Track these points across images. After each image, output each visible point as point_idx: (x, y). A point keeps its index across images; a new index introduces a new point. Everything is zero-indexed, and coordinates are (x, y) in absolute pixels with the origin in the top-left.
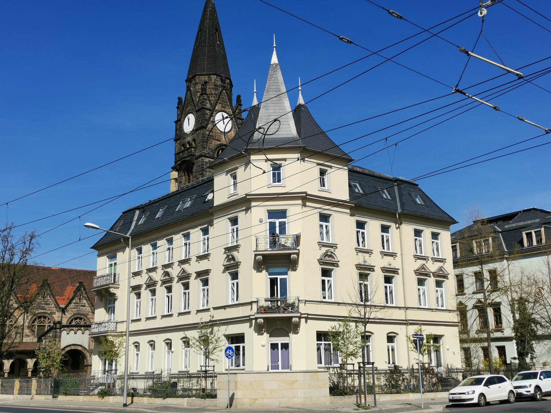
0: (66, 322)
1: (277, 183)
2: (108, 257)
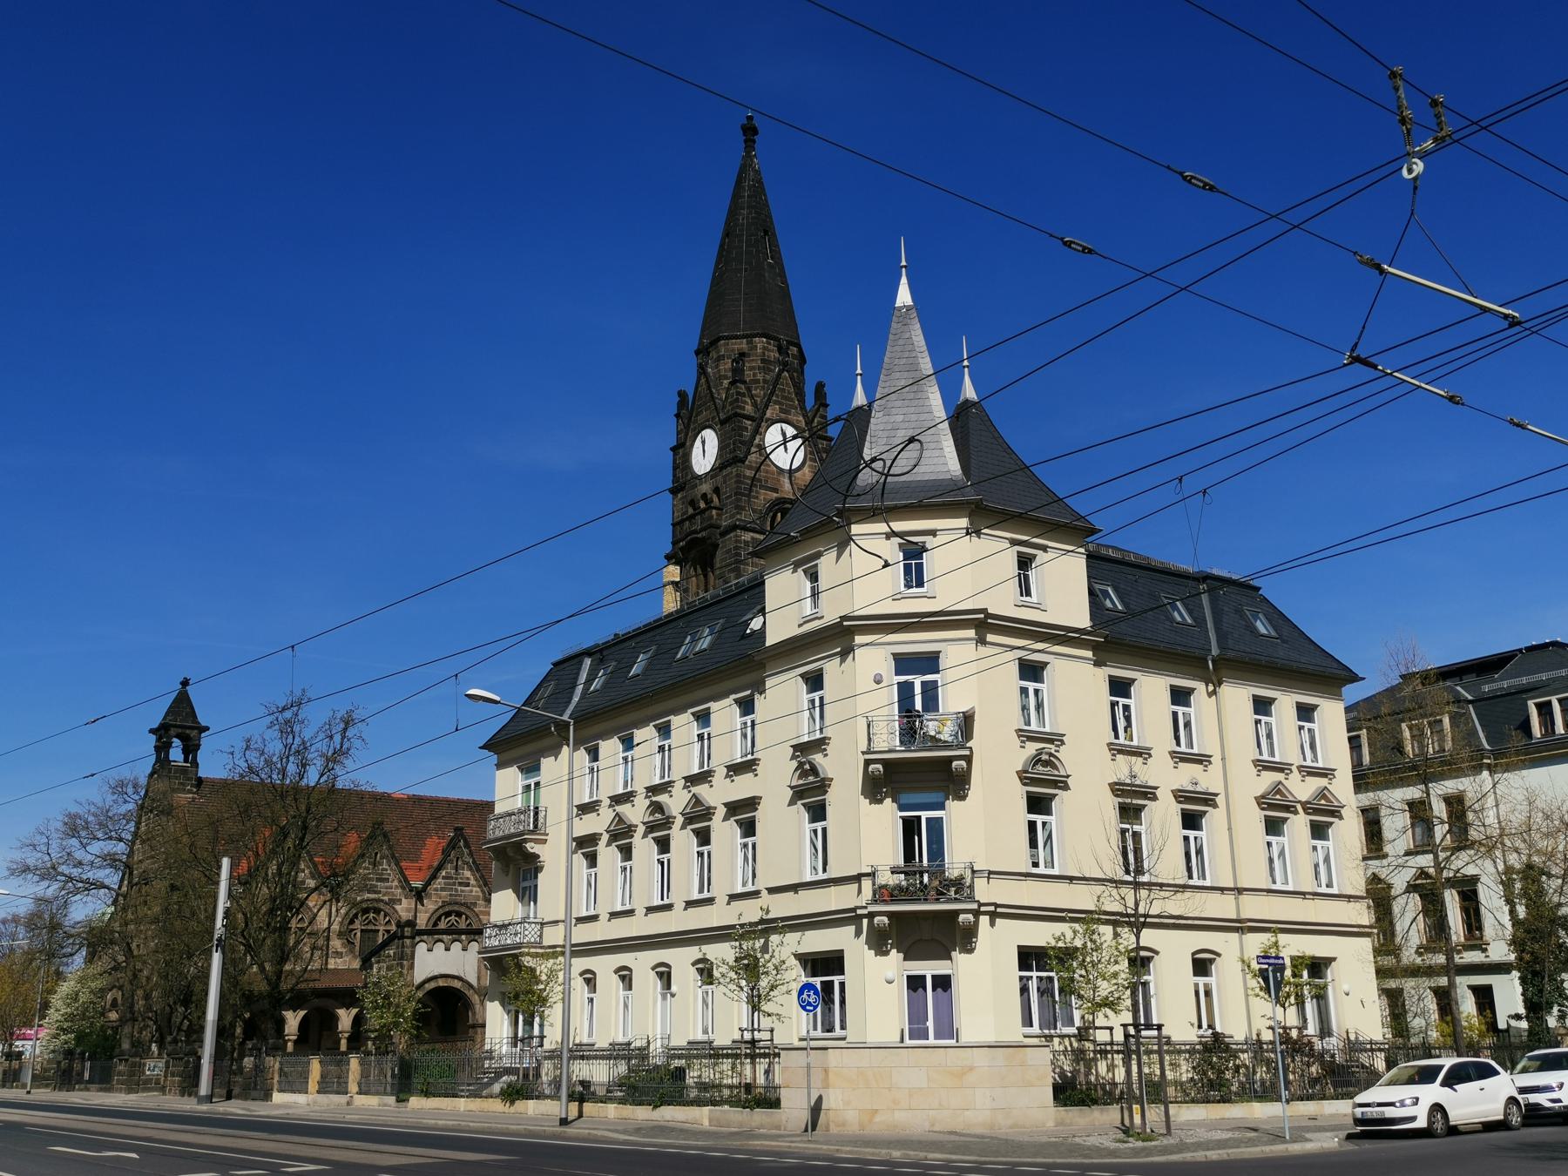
2: (521, 769)
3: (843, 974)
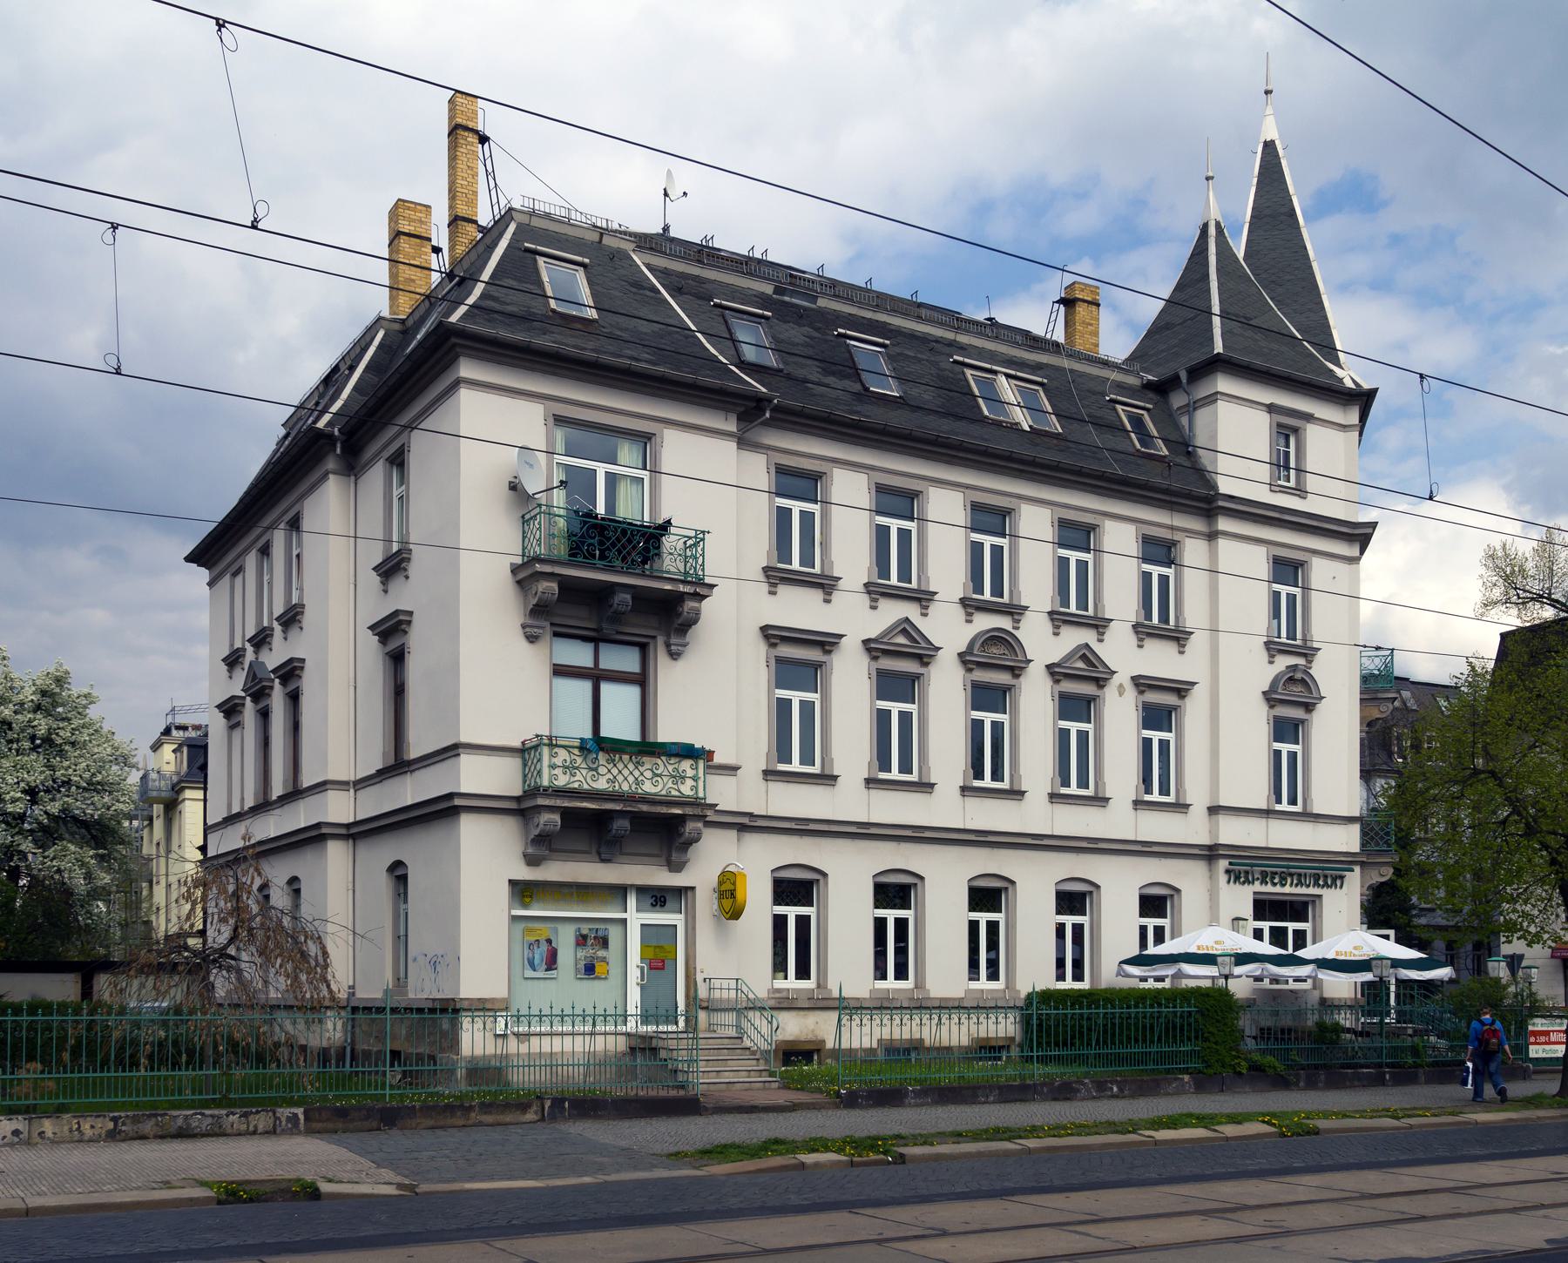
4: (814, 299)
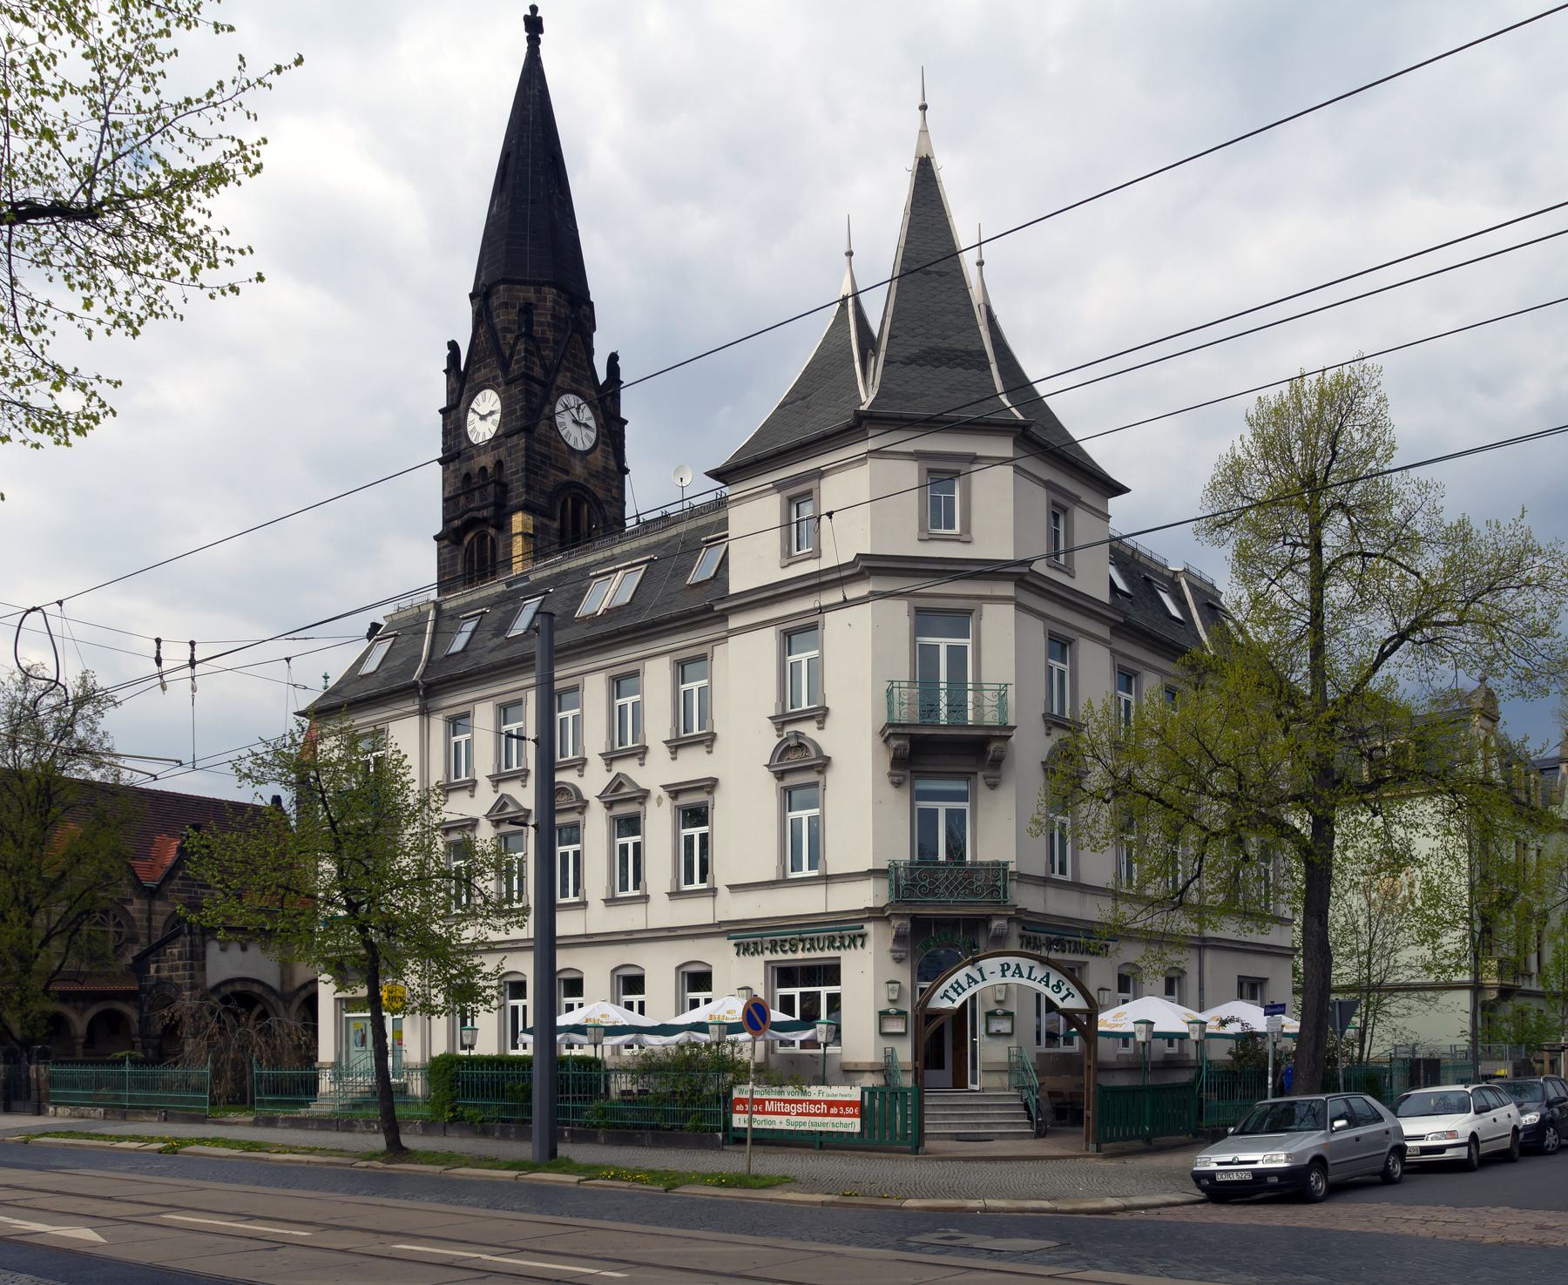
0: (162, 925)
1: (943, 531)
3: (710, 990)
4: (527, 579)
